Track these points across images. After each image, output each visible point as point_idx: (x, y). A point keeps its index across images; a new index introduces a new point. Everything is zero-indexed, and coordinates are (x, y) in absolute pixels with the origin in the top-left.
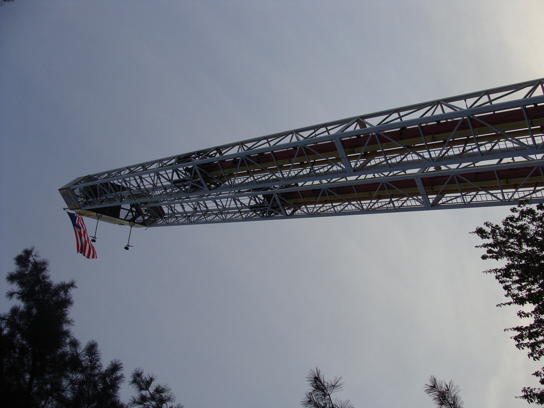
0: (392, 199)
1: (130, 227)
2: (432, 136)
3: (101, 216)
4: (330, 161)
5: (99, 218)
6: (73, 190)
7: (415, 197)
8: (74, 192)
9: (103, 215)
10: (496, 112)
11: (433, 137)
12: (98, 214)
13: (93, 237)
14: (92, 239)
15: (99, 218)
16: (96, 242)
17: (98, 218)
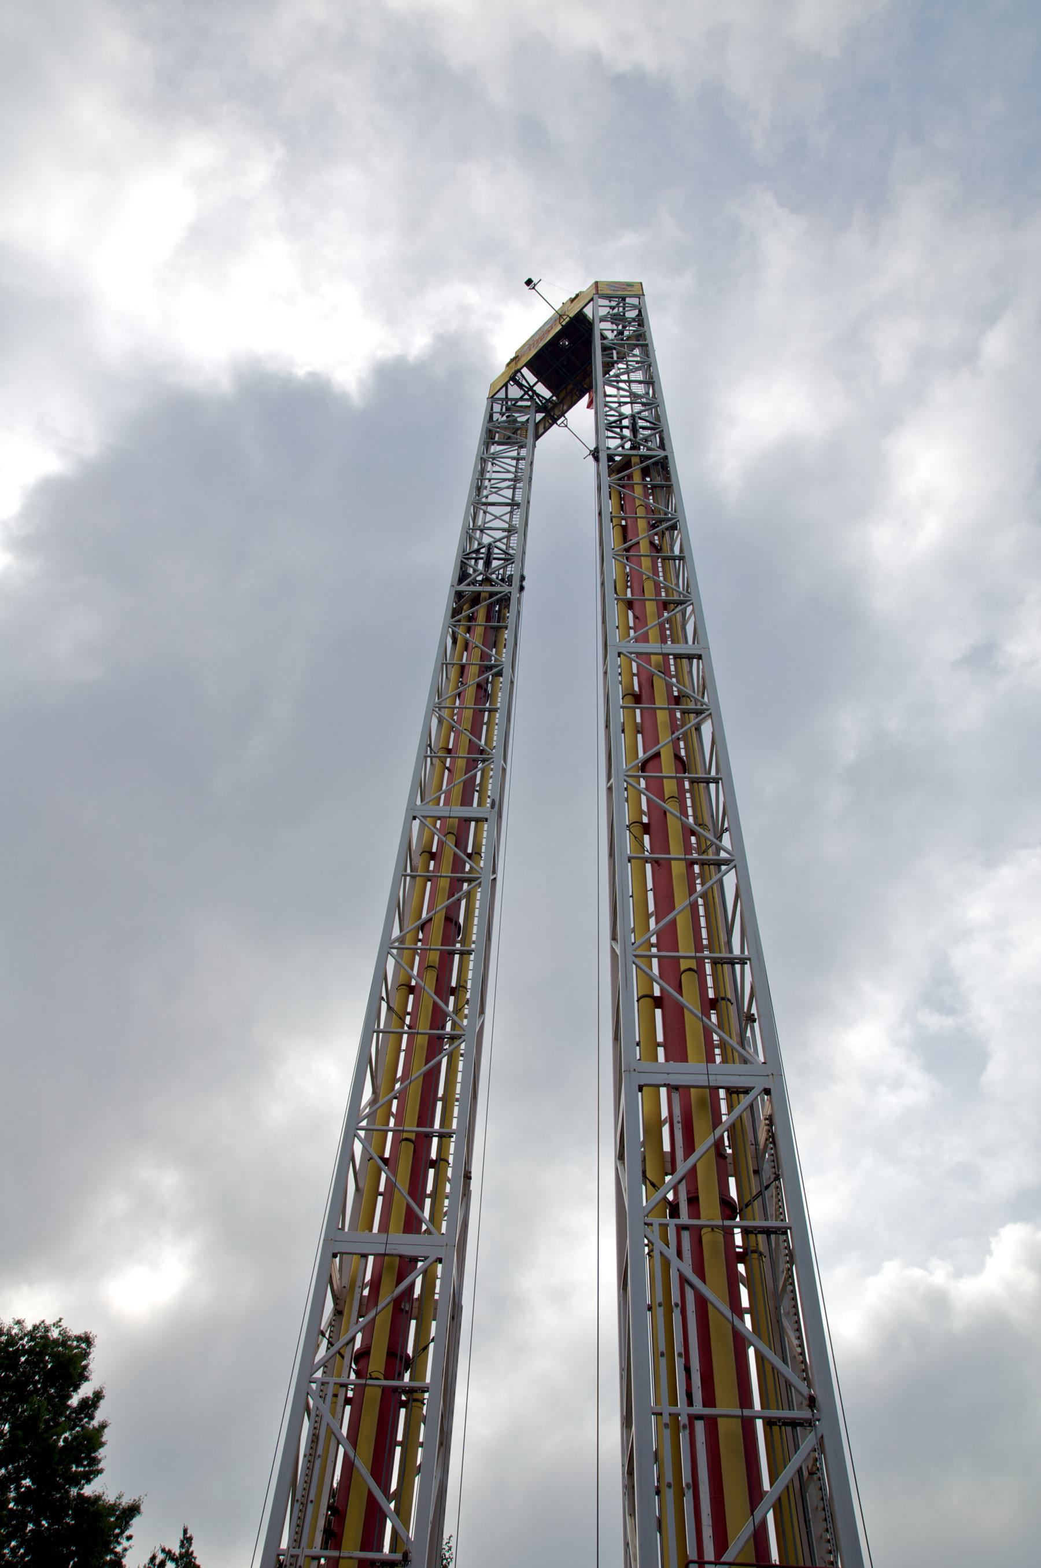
0: (373, 1257)
1: (534, 290)
2: (437, 966)
3: (561, 324)
4: (437, 794)
5: (560, 316)
6: (639, 298)
7: (411, 1362)
8: (637, 297)
9: (561, 327)
10: (398, 1449)
11: (435, 968)
12: (568, 319)
13: (535, 285)
14: (532, 281)
15: (560, 316)
16: (525, 285)
17: (560, 315)
